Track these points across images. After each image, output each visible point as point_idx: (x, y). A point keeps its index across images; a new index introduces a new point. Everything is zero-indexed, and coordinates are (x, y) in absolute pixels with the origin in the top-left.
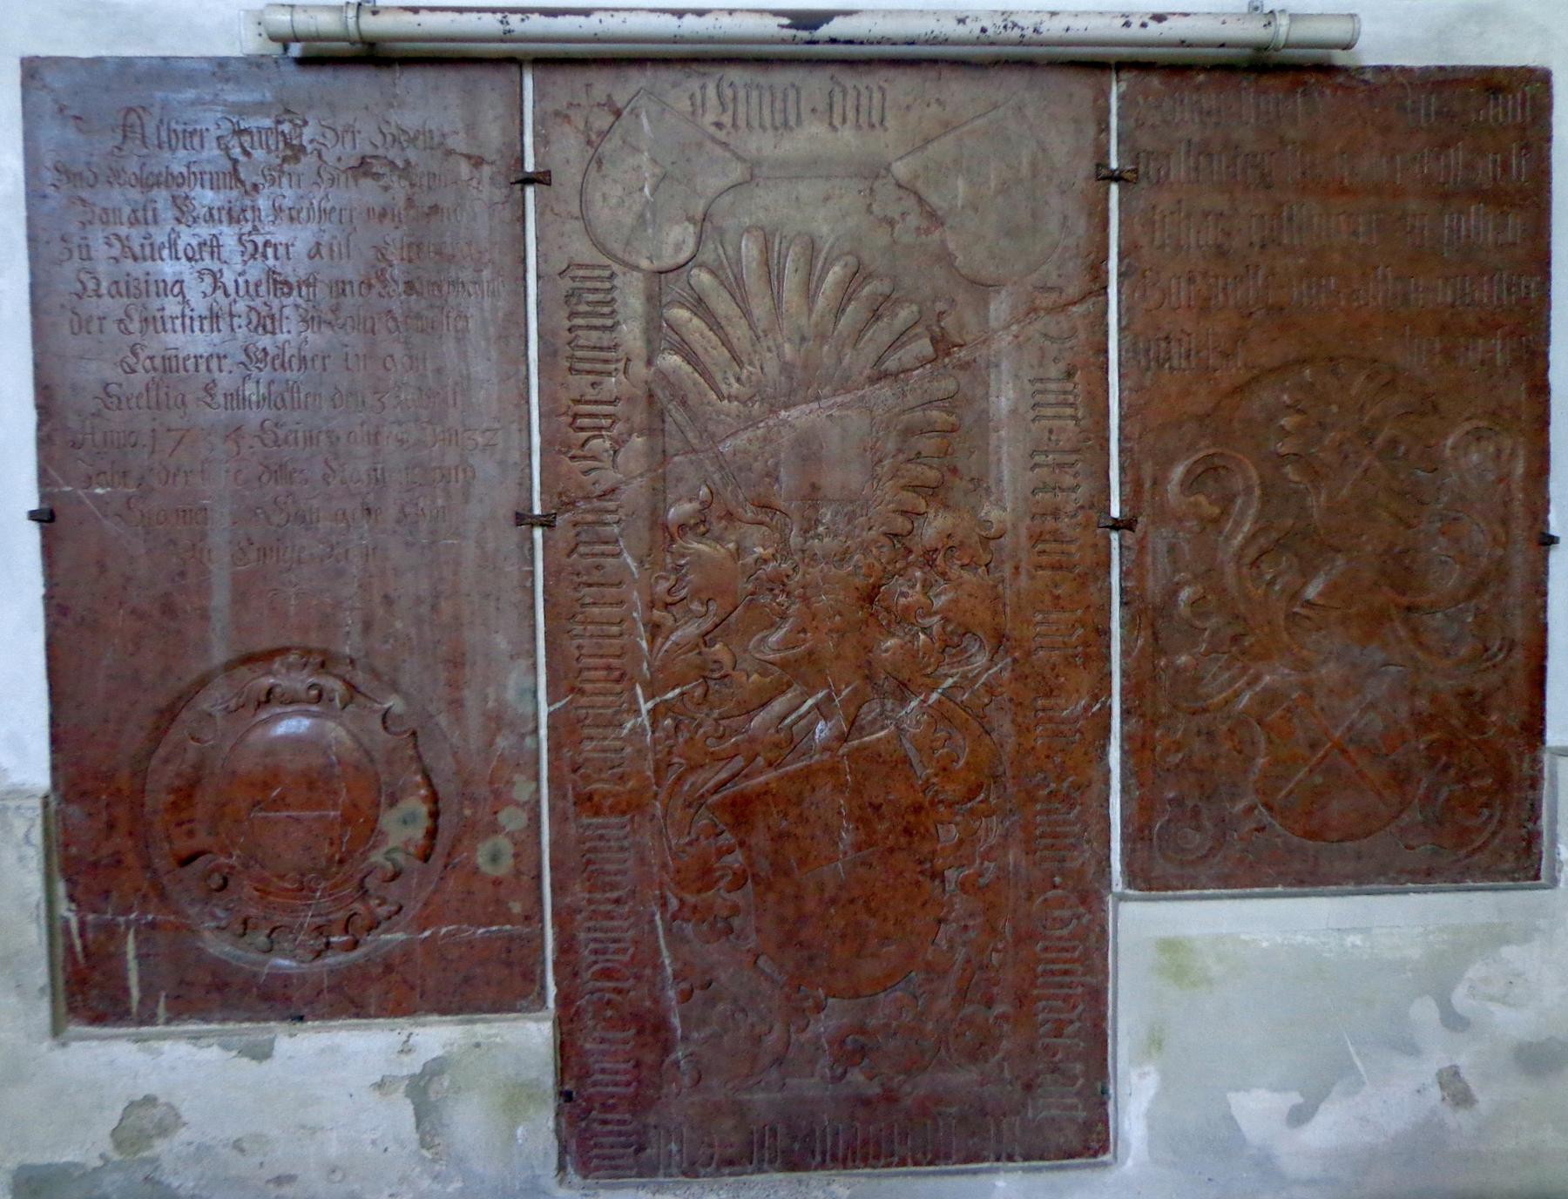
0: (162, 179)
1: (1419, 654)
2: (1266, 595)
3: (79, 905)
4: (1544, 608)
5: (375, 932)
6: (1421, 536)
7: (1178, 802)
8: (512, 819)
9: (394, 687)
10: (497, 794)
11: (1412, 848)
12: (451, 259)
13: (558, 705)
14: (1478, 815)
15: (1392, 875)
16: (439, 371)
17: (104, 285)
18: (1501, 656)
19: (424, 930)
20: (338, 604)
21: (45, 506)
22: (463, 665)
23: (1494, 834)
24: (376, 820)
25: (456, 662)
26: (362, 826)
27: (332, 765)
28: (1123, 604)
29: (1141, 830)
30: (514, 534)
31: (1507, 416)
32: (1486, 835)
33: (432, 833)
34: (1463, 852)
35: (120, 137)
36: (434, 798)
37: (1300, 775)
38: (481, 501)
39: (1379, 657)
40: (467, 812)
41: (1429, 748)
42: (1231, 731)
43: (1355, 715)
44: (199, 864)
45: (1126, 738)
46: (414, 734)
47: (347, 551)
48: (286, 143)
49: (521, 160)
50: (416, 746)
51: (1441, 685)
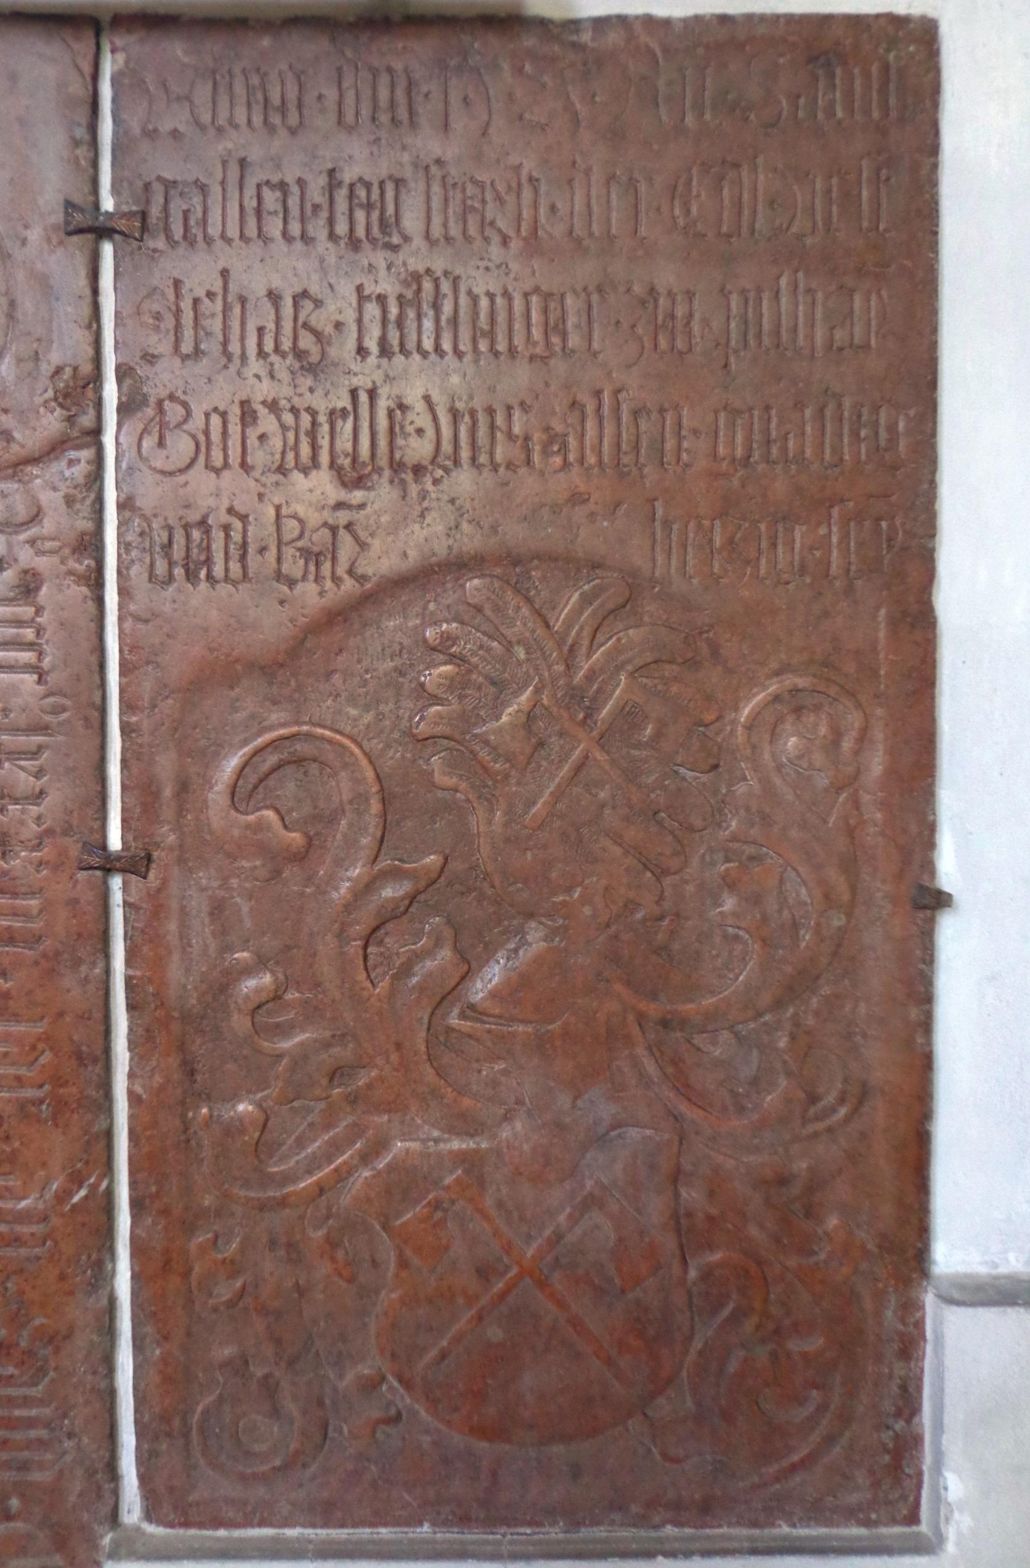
1: (683, 1107)
2: (392, 993)
4: (926, 1025)
6: (690, 888)
7: (239, 1366)
11: (677, 1461)
14: (801, 1401)
15: (635, 1509)
18: (843, 1111)
23: (830, 1440)
28: (131, 1007)
29: (165, 1418)
31: (850, 668)
32: (815, 1437)
34: (772, 1469)
37: (461, 1324)
39: (606, 1111)
41: (707, 1275)
42: (332, 1243)
43: (562, 1218)
45: (138, 1250)
51: (730, 1164)
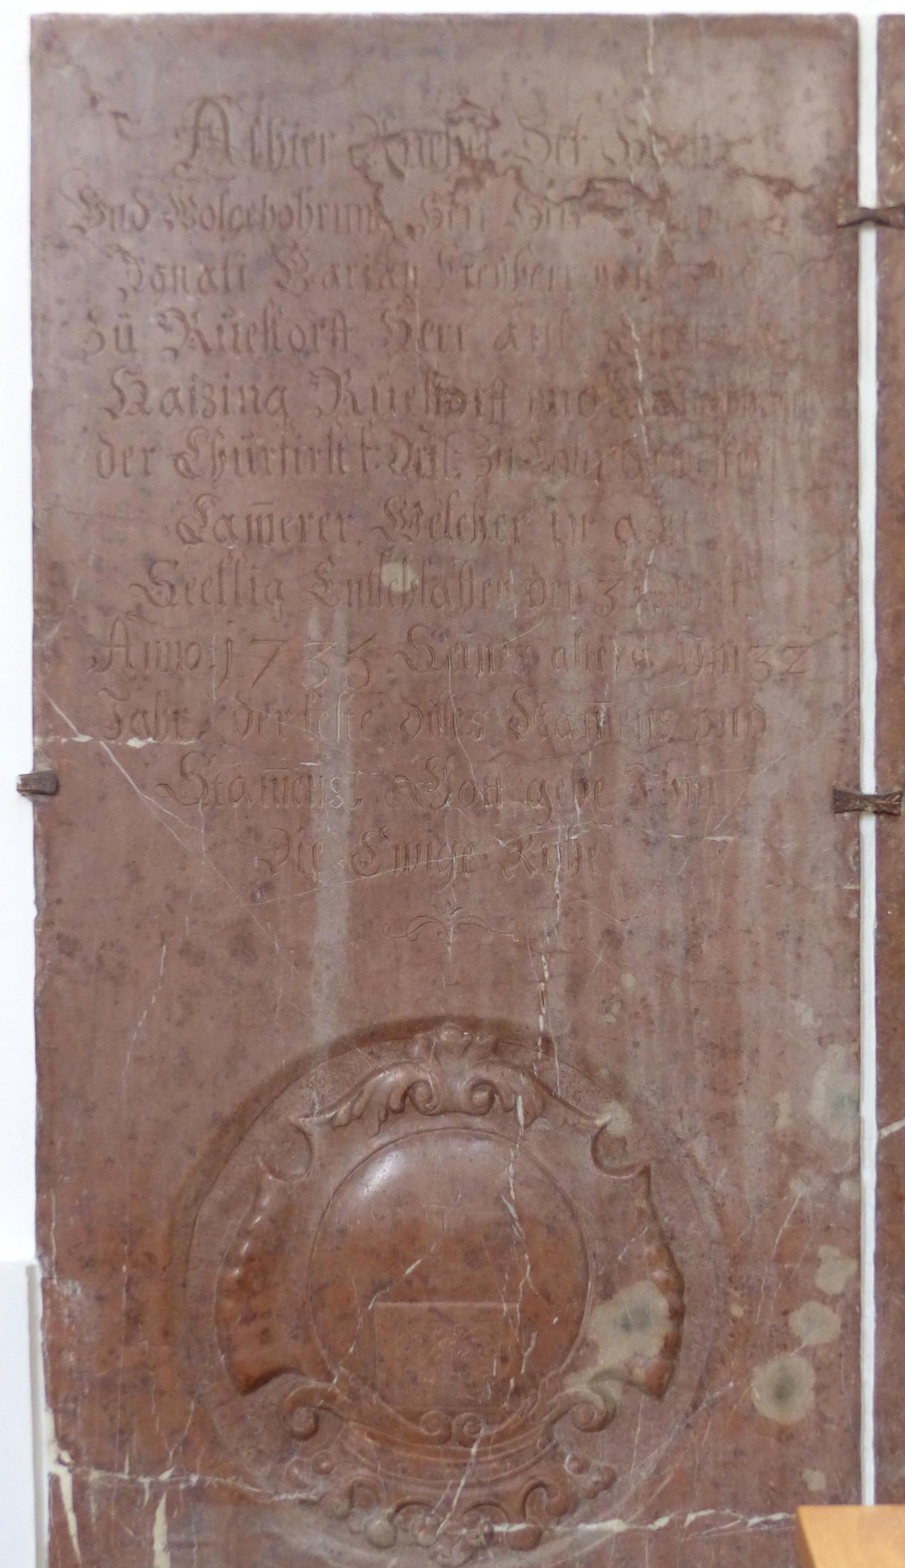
0: (257, 217)
3: (75, 1456)
5: (567, 1520)
8: (814, 1325)
9: (617, 1089)
10: (788, 1280)
12: (731, 352)
13: (896, 1127)
16: (711, 544)
17: (154, 393)
19: (657, 1517)
20: (527, 944)
21: (44, 767)
22: (737, 1052)
24: (579, 1322)
25: (727, 1048)
26: (556, 1329)
27: (510, 1223)
30: (826, 831)
33: (672, 1347)
35: (186, 148)
36: (676, 1286)
38: (775, 769)
40: (737, 1311)
44: (270, 1393)
46: (646, 1172)
47: (545, 853)
48: (463, 157)
49: (853, 186)
50: (648, 1194)
